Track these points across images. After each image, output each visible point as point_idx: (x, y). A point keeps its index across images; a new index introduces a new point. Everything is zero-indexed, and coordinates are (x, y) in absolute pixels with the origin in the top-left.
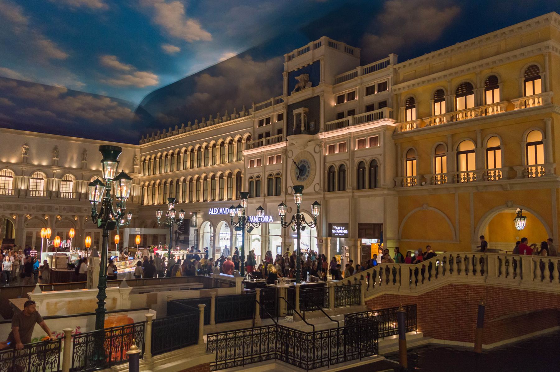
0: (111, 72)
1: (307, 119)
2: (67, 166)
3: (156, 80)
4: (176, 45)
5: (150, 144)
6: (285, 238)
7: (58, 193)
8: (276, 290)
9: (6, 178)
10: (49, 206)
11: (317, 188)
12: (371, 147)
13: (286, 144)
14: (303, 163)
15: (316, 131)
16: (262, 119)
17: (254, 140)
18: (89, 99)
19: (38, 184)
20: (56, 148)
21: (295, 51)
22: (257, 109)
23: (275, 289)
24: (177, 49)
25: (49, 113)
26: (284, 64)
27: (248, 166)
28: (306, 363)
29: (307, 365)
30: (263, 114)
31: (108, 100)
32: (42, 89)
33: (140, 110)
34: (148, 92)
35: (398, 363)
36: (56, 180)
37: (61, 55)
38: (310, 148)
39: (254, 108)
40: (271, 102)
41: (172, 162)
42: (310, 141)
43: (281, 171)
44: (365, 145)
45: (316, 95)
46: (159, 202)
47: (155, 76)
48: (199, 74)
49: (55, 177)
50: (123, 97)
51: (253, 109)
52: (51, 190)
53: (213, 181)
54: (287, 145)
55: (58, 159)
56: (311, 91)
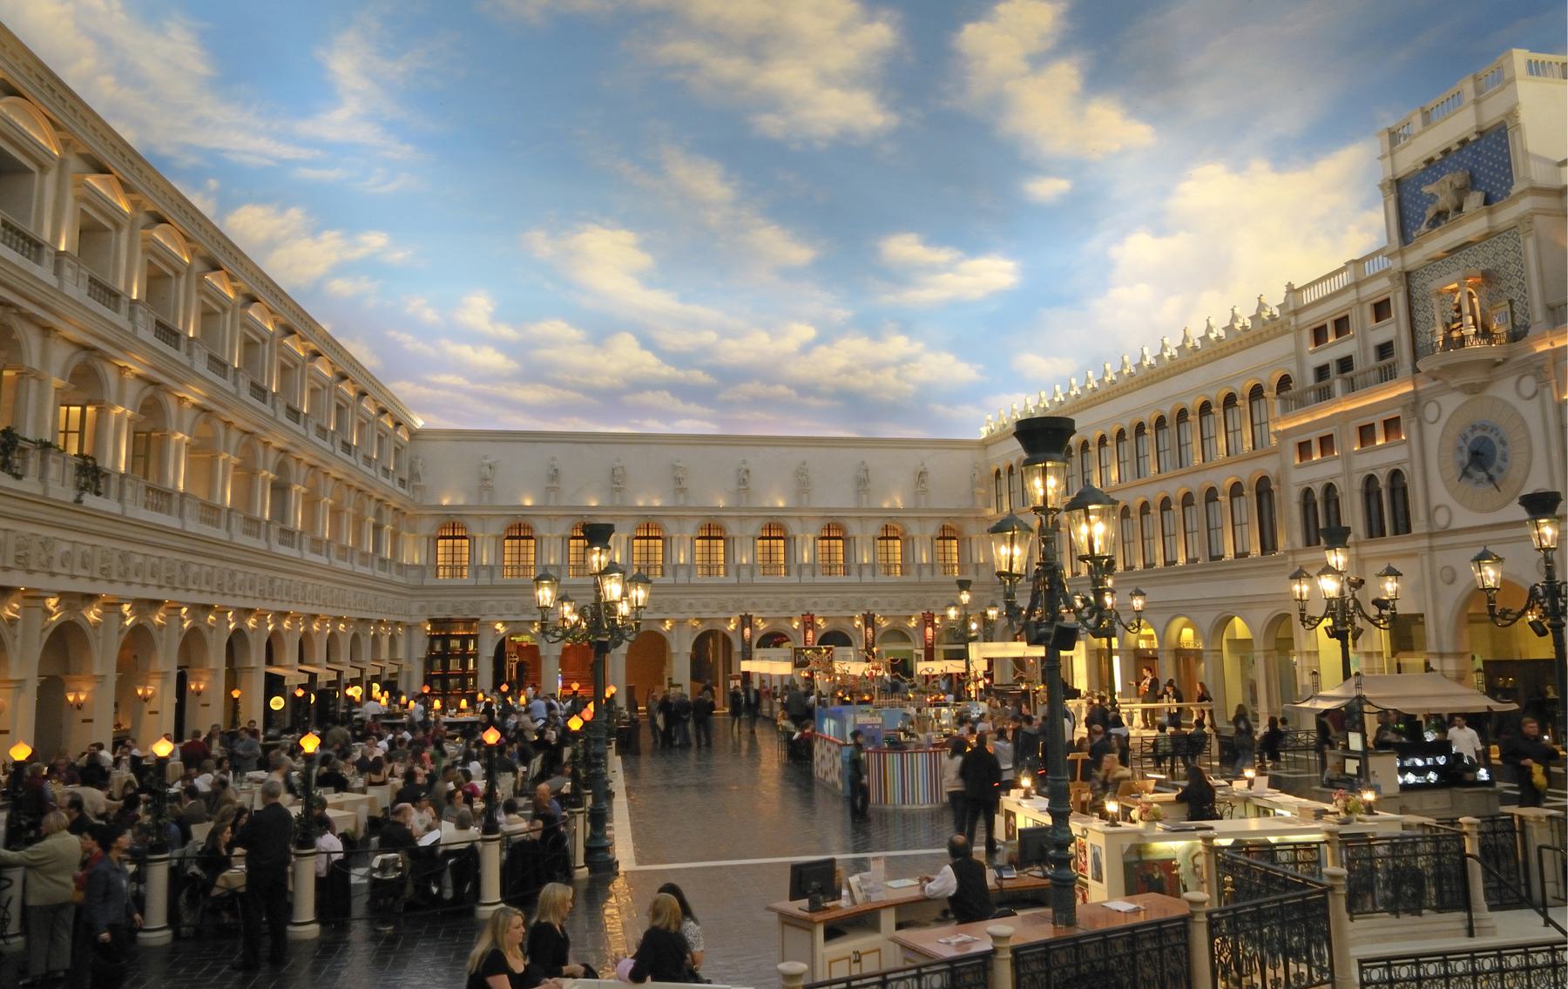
0: (900, 277)
1: (1480, 303)
8: (1516, 822)
10: (800, 598)
14: (1478, 433)
19: (651, 550)
23: (1513, 820)
35: (104, 823)
37: (800, 254)
41: (1085, 467)
43: (1407, 466)
46: (1191, 556)
47: (1009, 265)
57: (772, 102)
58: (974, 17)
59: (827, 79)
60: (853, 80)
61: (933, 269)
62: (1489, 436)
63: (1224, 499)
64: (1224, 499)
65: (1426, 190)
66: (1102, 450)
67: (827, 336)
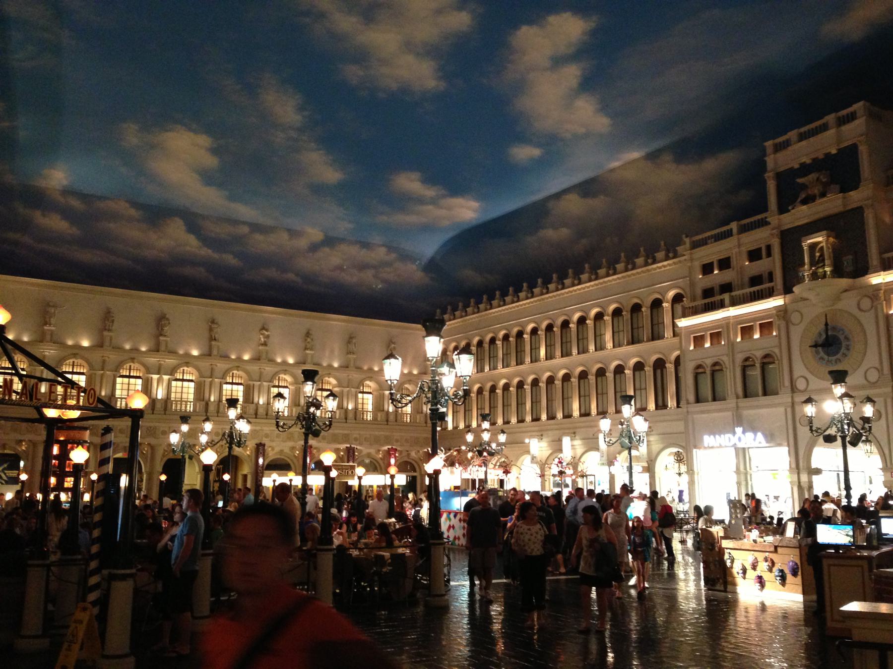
0: (404, 201)
3: (475, 211)
4: (538, 145)
5: (456, 323)
6: (799, 474)
9: (234, 386)
11: (873, 376)
12: (762, 337)
13: (785, 301)
15: (863, 270)
16: (711, 261)
17: (694, 299)
18: (354, 251)
19: (185, 390)
21: (793, 135)
22: (695, 245)
24: (536, 152)
25: (291, 276)
26: (766, 158)
27: (737, 338)
30: (713, 252)
32: (285, 236)
33: (431, 266)
34: (451, 234)
37: (332, 175)
38: (849, 303)
39: (690, 244)
40: (731, 230)
42: (846, 291)
43: (777, 351)
44: (704, 343)
45: (854, 205)
46: (443, 427)
47: (474, 204)
48: (558, 196)
50: (408, 246)
51: (688, 245)
53: (479, 396)
54: (786, 301)
55: (313, 352)
56: (841, 200)
57: (362, 57)
58: (530, 22)
59: (408, 46)
60: (431, 51)
61: (421, 201)
62: (837, 334)
63: (592, 378)
64: (592, 378)
65: (800, 180)
66: (533, 337)
67: (330, 241)
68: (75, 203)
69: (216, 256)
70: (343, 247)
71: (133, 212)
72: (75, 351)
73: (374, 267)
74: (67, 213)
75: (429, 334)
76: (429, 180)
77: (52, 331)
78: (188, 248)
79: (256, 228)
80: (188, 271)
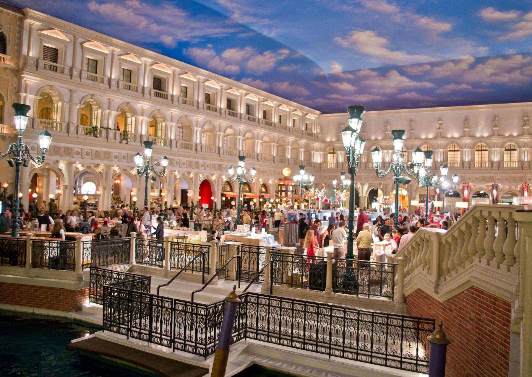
2: (478, 135)
7: (500, 163)
18: (499, 62)
19: (455, 156)
20: (466, 120)
25: (464, 86)
28: (204, 347)
29: (206, 349)
31: (519, 58)
32: (452, 65)
36: (440, 152)
37: (445, 27)
49: (526, 146)
52: (523, 160)
68: (350, 76)
69: (419, 84)
70: (490, 62)
71: (373, 73)
72: (452, 140)
73: (518, 69)
74: (349, 81)
75: (352, 117)
76: (503, 7)
77: (365, 135)
78: (404, 84)
79: (433, 64)
80: (408, 95)
